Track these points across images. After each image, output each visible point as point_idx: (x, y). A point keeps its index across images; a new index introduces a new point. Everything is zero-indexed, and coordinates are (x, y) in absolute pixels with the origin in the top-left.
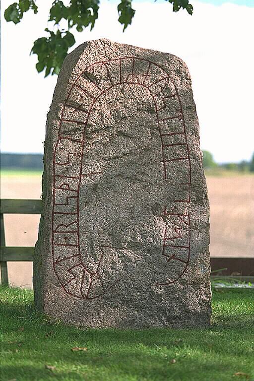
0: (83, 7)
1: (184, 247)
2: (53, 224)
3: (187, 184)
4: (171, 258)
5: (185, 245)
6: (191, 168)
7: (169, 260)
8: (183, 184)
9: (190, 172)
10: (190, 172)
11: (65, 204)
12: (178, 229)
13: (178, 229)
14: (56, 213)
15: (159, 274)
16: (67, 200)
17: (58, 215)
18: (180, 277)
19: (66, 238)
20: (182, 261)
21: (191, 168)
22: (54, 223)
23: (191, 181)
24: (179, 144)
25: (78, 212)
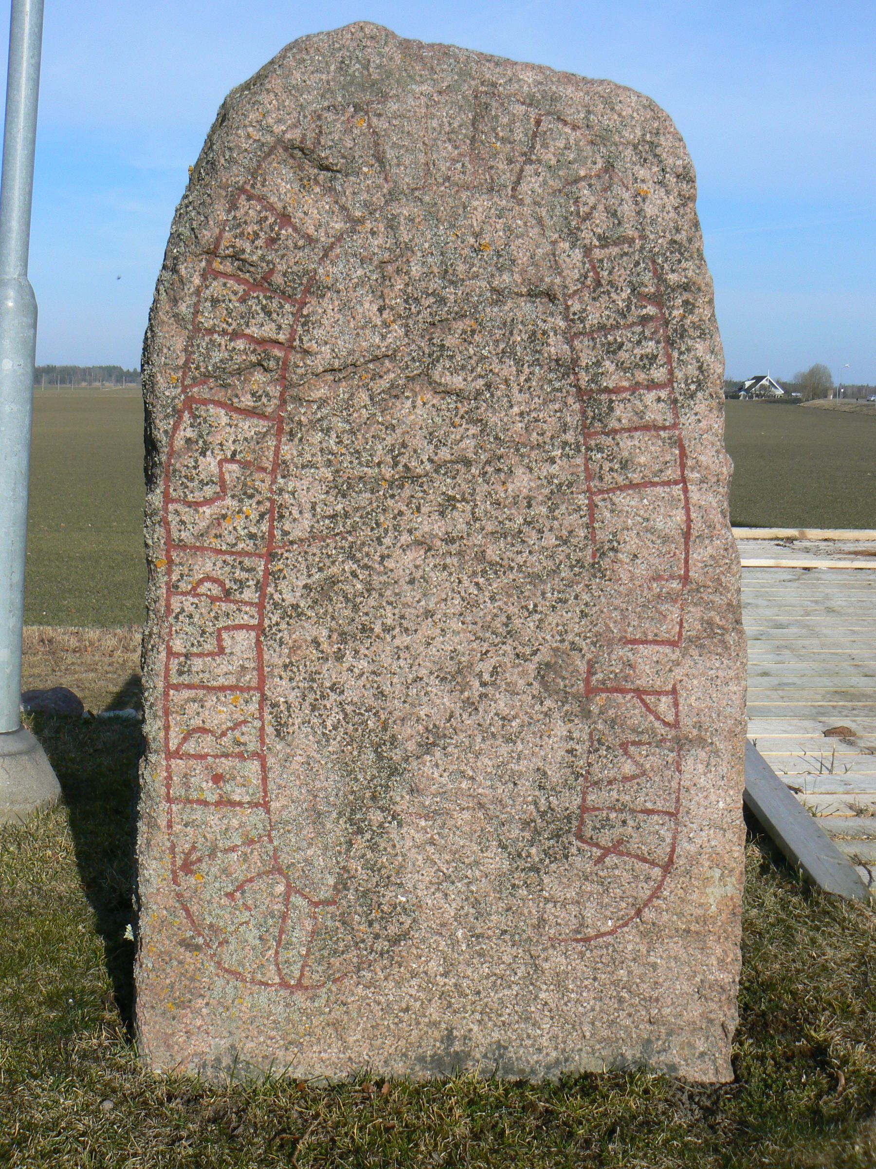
0: (840, 1163)
1: (658, 812)
2: (167, 728)
3: (672, 577)
4: (607, 851)
5: (659, 806)
6: (689, 520)
7: (600, 860)
8: (657, 578)
9: (687, 535)
10: (687, 535)
11: (211, 654)
12: (634, 743)
13: (634, 743)
14: (177, 687)
15: (564, 906)
16: (219, 639)
17: (186, 694)
18: (639, 913)
19: (217, 779)
20: (645, 860)
21: (689, 520)
22: (172, 723)
23: (687, 571)
24: (646, 428)
25: (262, 679)
